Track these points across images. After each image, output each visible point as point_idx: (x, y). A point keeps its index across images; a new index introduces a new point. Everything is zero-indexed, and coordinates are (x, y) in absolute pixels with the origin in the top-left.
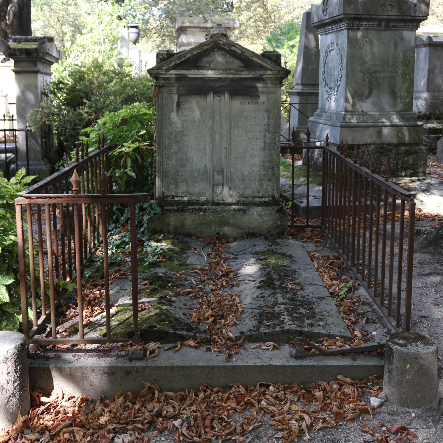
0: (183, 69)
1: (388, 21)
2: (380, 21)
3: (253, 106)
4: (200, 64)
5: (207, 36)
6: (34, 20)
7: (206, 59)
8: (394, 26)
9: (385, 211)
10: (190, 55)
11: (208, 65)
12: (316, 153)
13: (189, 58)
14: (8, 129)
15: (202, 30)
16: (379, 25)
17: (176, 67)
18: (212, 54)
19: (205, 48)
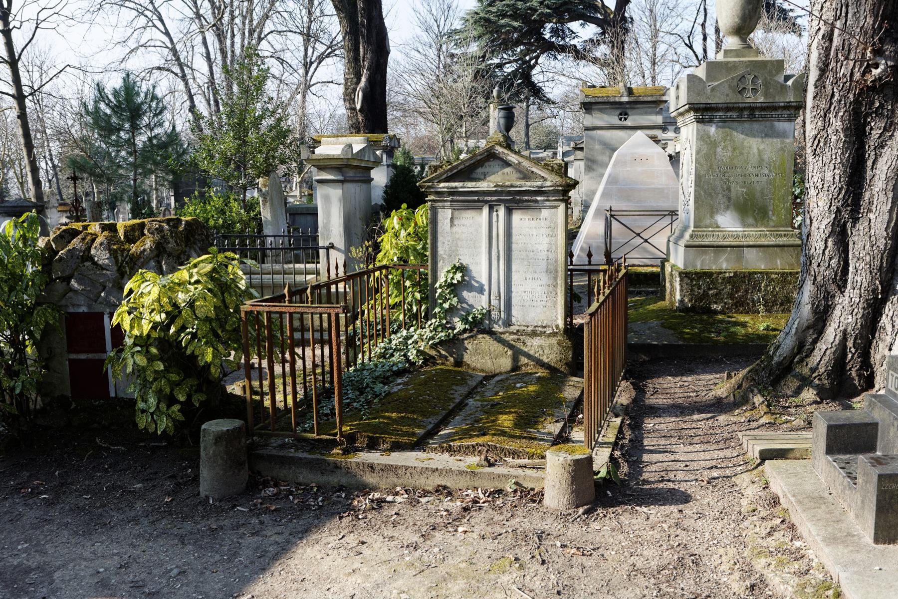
0: (455, 182)
1: (752, 109)
2: (741, 110)
3: (534, 223)
4: (474, 176)
5: (621, 114)
6: (401, 107)
7: (480, 170)
8: (761, 116)
9: (687, 333)
10: (463, 166)
11: (482, 177)
12: (76, 285)
13: (461, 170)
14: (271, 234)
15: (614, 106)
16: (741, 116)
17: (447, 180)
18: (487, 164)
19: (479, 158)
